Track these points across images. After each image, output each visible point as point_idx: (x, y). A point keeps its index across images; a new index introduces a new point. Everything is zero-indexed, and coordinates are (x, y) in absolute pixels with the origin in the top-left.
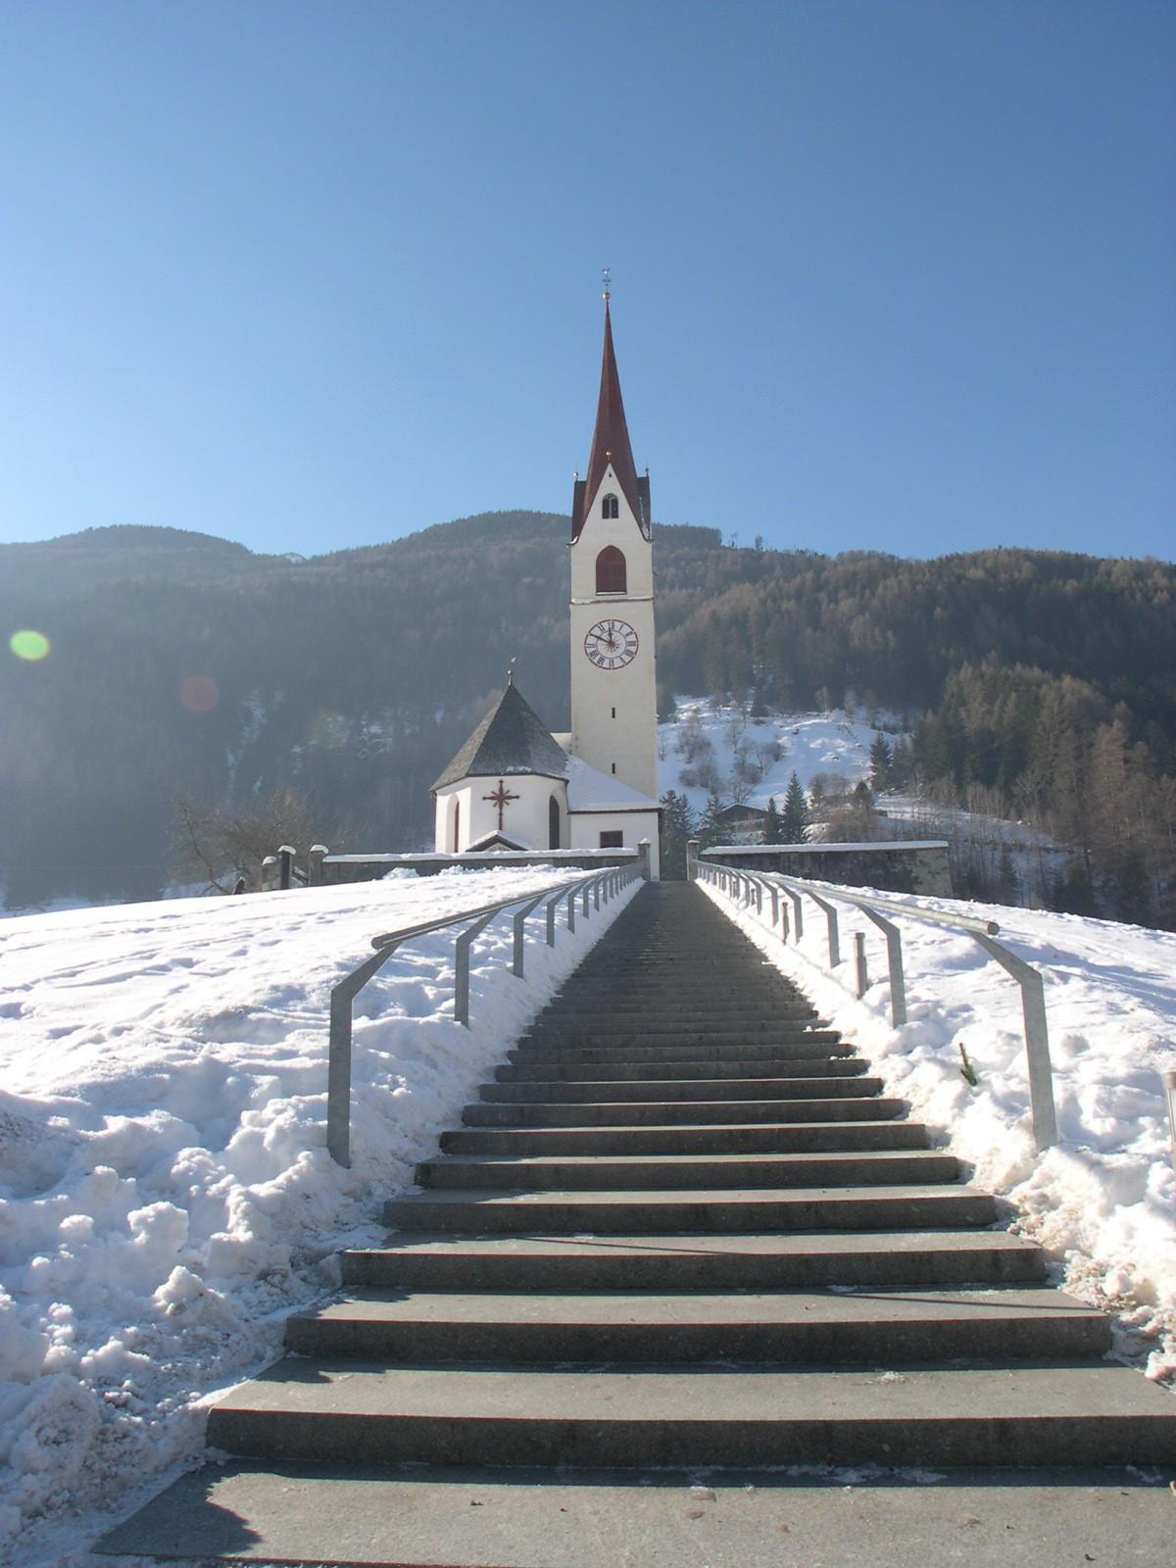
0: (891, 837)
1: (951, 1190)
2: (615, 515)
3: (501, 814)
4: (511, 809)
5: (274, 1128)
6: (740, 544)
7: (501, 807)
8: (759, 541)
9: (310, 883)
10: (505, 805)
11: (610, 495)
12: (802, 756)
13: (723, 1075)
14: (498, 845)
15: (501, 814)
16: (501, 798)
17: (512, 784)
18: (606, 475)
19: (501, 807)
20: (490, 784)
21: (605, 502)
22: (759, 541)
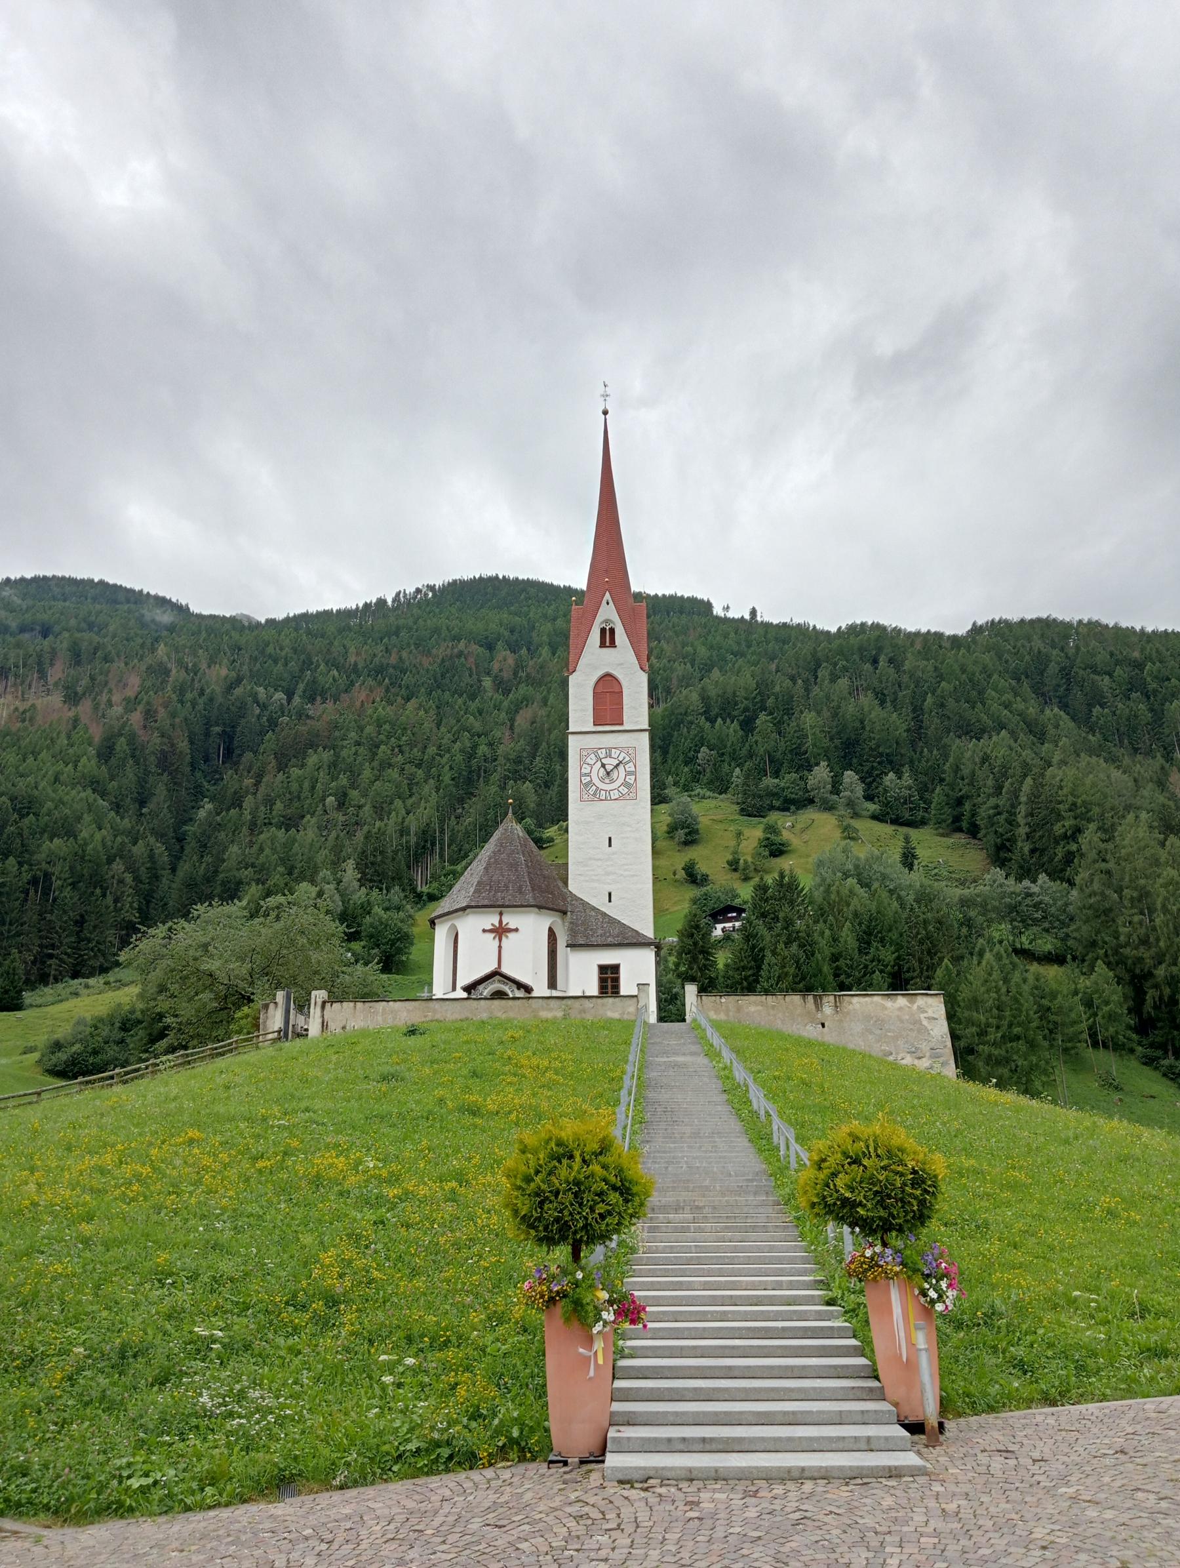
0: (962, 1044)
1: (931, 1375)
2: (613, 644)
3: (500, 947)
4: (509, 941)
5: (687, 859)
6: (733, 614)
7: (500, 940)
8: (753, 612)
9: (424, 977)
10: (504, 939)
11: (607, 621)
12: (944, 1284)
13: (661, 1302)
14: (498, 977)
15: (500, 947)
16: (500, 931)
17: (511, 920)
18: (604, 602)
19: (500, 940)
20: (491, 920)
21: (603, 631)
22: (753, 612)
